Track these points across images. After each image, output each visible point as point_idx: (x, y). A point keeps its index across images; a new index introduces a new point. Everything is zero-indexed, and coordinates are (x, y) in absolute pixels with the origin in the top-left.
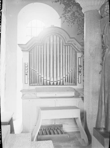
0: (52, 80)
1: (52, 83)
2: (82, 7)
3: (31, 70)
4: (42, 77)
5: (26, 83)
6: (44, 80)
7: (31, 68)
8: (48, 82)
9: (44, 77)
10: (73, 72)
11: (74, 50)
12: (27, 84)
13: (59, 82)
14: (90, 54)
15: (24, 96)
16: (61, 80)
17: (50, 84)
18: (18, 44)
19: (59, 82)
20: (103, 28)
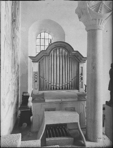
0: (58, 85)
1: (58, 88)
2: (76, 14)
3: (40, 77)
4: (49, 83)
5: (36, 88)
6: (63, 86)
7: (40, 76)
8: (55, 87)
9: (51, 84)
10: (76, 78)
11: (77, 61)
12: (37, 89)
13: (64, 87)
14: (92, 68)
15: (34, 100)
16: (63, 86)
17: (56, 89)
18: (29, 57)
19: (64, 87)
20: (82, 11)
